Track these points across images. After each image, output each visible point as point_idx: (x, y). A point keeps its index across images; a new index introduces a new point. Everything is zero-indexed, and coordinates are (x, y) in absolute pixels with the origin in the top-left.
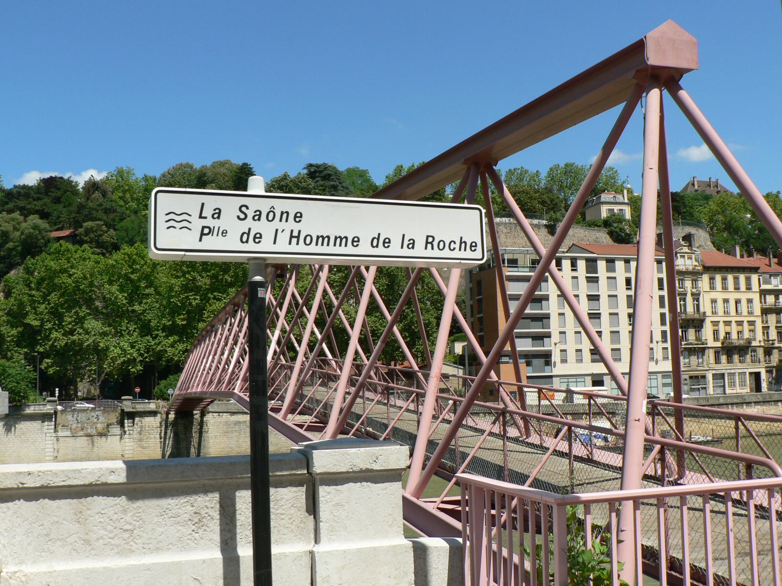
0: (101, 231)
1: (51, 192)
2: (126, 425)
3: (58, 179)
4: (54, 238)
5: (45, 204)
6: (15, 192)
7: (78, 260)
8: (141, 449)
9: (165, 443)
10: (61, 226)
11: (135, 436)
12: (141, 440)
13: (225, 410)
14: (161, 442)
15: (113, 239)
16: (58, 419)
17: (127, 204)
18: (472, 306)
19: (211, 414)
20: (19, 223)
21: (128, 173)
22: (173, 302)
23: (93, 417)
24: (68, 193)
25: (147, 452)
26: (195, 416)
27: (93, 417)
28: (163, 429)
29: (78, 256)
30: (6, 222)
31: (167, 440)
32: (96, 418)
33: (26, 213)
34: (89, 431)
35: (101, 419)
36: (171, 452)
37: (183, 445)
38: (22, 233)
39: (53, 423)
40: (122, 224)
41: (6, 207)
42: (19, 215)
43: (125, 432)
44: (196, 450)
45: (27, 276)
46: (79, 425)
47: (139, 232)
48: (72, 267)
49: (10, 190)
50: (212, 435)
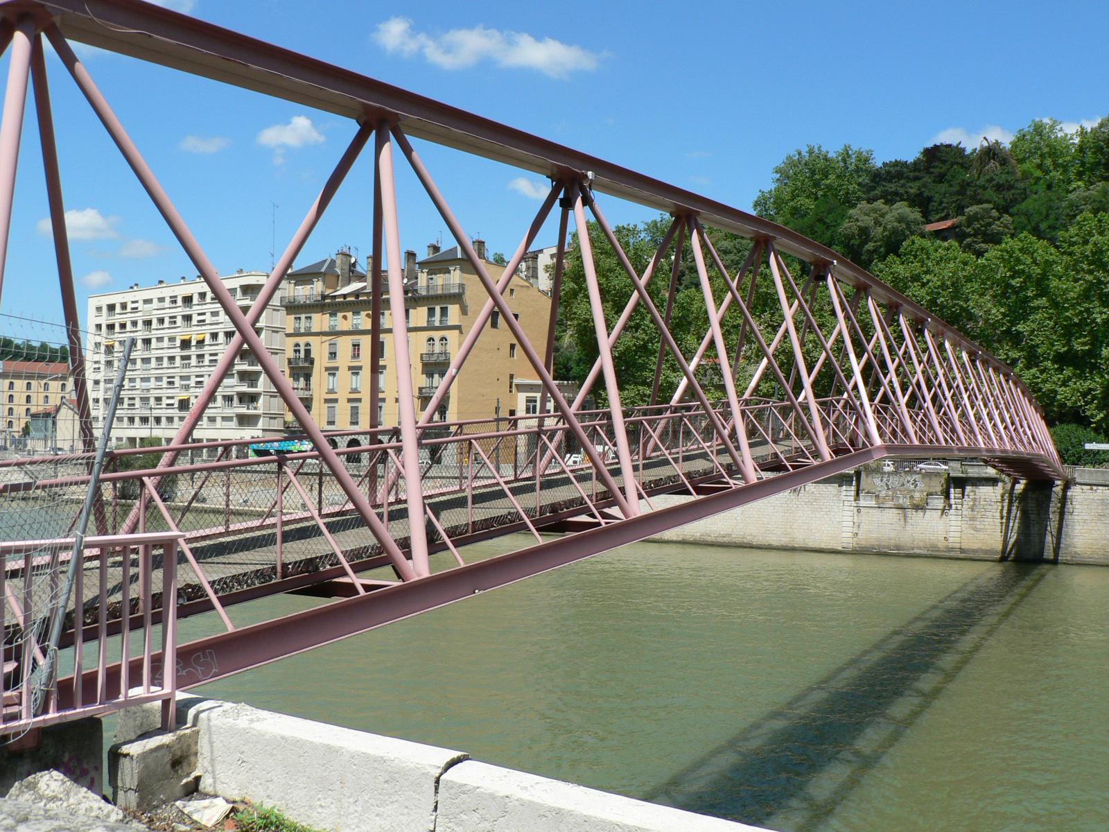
0: (990, 217)
1: (934, 167)
2: (952, 496)
3: (942, 148)
4: (930, 232)
5: (925, 186)
6: (883, 172)
8: (974, 532)
9: (1007, 526)
10: (943, 215)
11: (964, 513)
12: (973, 519)
14: (1002, 523)
16: (862, 483)
18: (925, 401)
19: (1078, 487)
20: (883, 216)
23: (908, 482)
24: (955, 166)
25: (981, 535)
26: (1054, 489)
27: (908, 482)
28: (1006, 504)
30: (866, 214)
31: (1011, 521)
32: (913, 484)
33: (890, 199)
34: (901, 501)
35: (921, 485)
36: (1017, 539)
37: (1035, 530)
39: (853, 488)
41: (873, 194)
43: (950, 506)
44: (1054, 539)
46: (890, 493)
48: (926, 273)
50: (1079, 518)
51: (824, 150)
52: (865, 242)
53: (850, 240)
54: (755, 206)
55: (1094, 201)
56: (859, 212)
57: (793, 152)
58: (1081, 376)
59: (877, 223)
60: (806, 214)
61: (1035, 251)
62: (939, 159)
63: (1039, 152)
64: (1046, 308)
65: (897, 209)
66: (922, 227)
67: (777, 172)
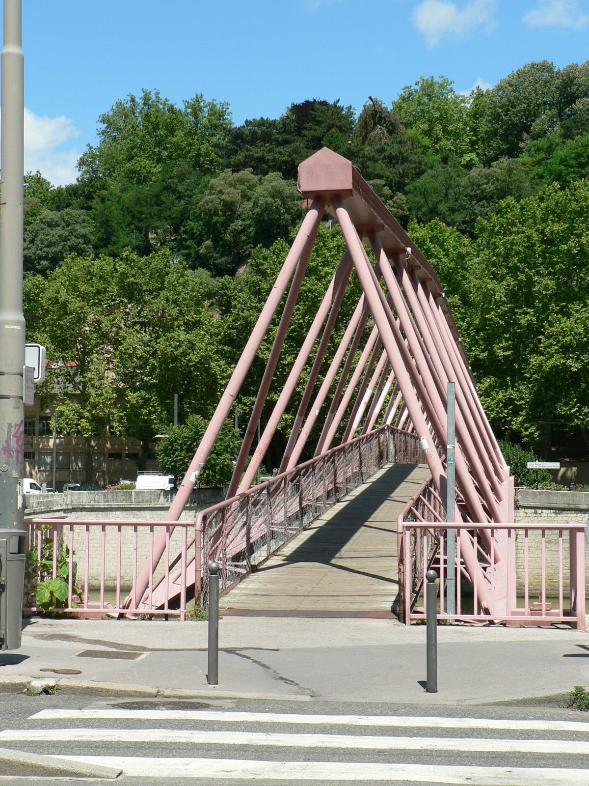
1: (306, 128)
6: (247, 132)
7: (334, 252)
13: (546, 505)
15: (403, 210)
17: (437, 143)
20: (251, 188)
21: (441, 86)
22: (491, 320)
29: (335, 244)
30: (231, 185)
38: (256, 204)
40: (418, 183)
41: (233, 159)
42: (252, 173)
45: (256, 278)
47: (446, 195)
49: (239, 129)
51: (162, 97)
52: (231, 219)
53: (211, 216)
54: (80, 165)
55: (498, 180)
56: (222, 182)
57: (124, 98)
58: (503, 386)
59: (245, 197)
60: (146, 179)
61: (445, 241)
62: (313, 120)
63: (427, 116)
64: (458, 307)
65: (271, 181)
66: (299, 203)
67: (103, 121)
